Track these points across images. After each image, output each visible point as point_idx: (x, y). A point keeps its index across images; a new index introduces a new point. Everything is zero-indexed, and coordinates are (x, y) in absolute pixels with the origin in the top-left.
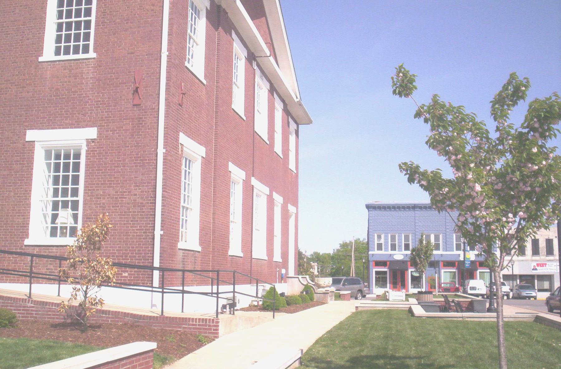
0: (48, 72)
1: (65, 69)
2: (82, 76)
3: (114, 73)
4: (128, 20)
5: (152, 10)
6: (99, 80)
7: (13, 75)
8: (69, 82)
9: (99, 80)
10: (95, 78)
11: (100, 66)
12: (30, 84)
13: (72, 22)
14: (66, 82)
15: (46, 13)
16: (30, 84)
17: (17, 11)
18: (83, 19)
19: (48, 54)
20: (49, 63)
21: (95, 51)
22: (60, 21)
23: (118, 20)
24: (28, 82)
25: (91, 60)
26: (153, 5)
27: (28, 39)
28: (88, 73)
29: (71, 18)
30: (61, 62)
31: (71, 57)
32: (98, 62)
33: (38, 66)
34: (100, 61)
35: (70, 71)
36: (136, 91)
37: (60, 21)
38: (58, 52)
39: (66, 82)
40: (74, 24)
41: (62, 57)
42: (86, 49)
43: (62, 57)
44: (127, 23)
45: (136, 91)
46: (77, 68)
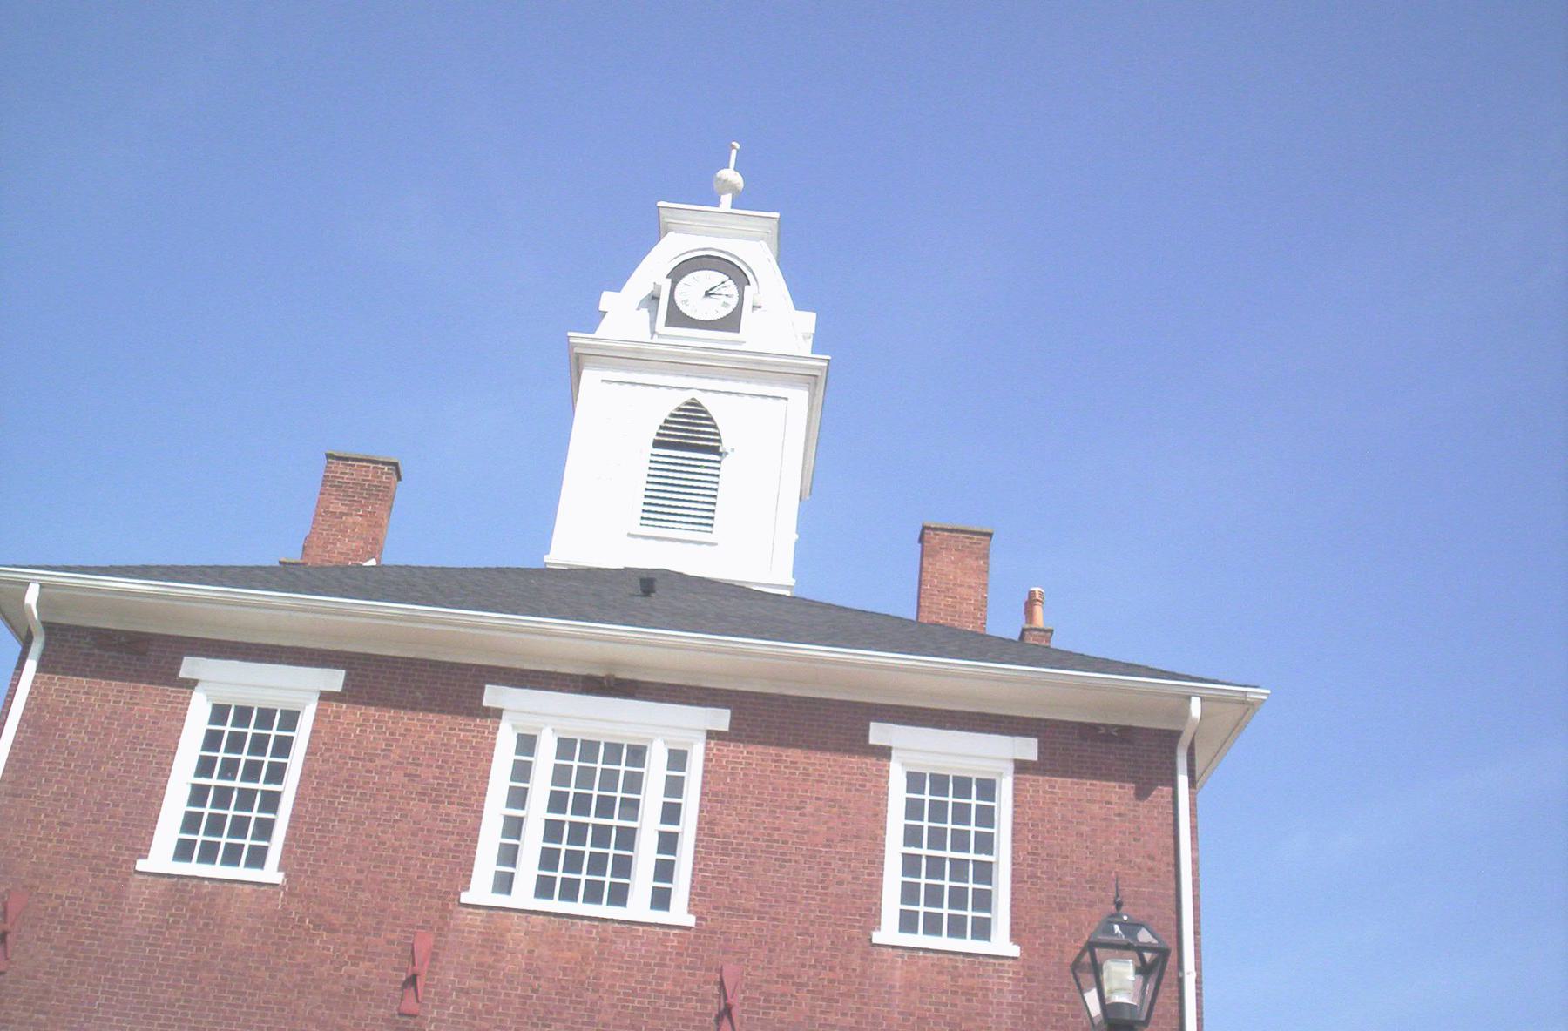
0: (898, 973)
1: (940, 973)
2: (985, 996)
3: (1067, 1002)
4: (1092, 881)
5: (1151, 869)
6: (1029, 1012)
7: (803, 966)
8: (955, 1006)
9: (1029, 1012)
10: (1019, 1005)
11: (1030, 980)
12: (847, 995)
13: (255, 791)
14: (945, 1005)
15: (884, 828)
16: (847, 995)
17: (809, 809)
18: (261, 786)
19: (160, 858)
20: (900, 952)
21: (1015, 936)
22: (203, 781)
23: (1068, 878)
24: (843, 989)
25: (610, 926)
26: (1152, 858)
27: (841, 883)
28: (1000, 991)
29: (564, 812)
30: (931, 954)
31: (579, 908)
32: (1026, 970)
33: (869, 953)
34: (1031, 968)
35: (954, 979)
36: (412, 981)
37: (203, 781)
38: (183, 851)
39: (945, 1005)
40: (212, 792)
41: (555, 905)
42: (257, 858)
43: (555, 905)
44: (1092, 889)
45: (412, 981)
46: (972, 976)
